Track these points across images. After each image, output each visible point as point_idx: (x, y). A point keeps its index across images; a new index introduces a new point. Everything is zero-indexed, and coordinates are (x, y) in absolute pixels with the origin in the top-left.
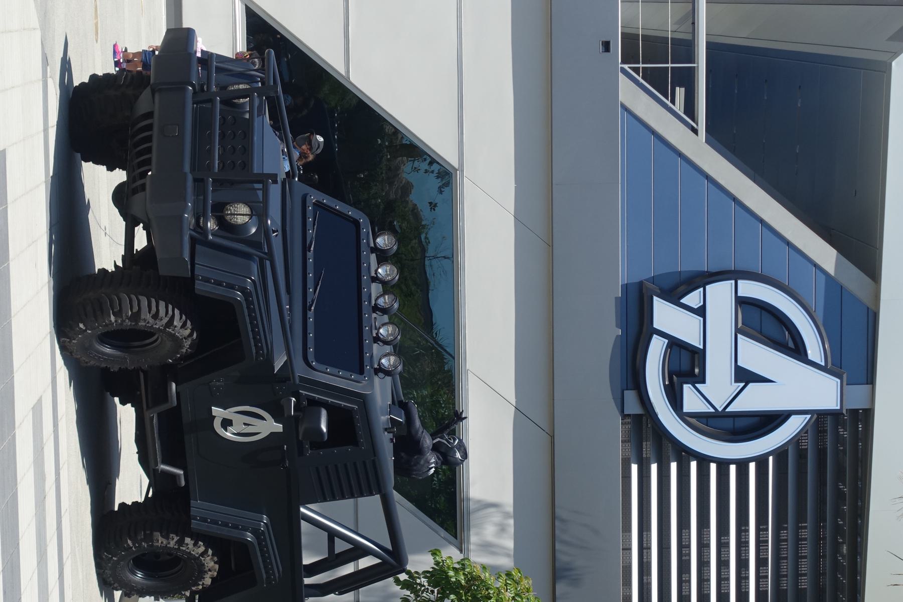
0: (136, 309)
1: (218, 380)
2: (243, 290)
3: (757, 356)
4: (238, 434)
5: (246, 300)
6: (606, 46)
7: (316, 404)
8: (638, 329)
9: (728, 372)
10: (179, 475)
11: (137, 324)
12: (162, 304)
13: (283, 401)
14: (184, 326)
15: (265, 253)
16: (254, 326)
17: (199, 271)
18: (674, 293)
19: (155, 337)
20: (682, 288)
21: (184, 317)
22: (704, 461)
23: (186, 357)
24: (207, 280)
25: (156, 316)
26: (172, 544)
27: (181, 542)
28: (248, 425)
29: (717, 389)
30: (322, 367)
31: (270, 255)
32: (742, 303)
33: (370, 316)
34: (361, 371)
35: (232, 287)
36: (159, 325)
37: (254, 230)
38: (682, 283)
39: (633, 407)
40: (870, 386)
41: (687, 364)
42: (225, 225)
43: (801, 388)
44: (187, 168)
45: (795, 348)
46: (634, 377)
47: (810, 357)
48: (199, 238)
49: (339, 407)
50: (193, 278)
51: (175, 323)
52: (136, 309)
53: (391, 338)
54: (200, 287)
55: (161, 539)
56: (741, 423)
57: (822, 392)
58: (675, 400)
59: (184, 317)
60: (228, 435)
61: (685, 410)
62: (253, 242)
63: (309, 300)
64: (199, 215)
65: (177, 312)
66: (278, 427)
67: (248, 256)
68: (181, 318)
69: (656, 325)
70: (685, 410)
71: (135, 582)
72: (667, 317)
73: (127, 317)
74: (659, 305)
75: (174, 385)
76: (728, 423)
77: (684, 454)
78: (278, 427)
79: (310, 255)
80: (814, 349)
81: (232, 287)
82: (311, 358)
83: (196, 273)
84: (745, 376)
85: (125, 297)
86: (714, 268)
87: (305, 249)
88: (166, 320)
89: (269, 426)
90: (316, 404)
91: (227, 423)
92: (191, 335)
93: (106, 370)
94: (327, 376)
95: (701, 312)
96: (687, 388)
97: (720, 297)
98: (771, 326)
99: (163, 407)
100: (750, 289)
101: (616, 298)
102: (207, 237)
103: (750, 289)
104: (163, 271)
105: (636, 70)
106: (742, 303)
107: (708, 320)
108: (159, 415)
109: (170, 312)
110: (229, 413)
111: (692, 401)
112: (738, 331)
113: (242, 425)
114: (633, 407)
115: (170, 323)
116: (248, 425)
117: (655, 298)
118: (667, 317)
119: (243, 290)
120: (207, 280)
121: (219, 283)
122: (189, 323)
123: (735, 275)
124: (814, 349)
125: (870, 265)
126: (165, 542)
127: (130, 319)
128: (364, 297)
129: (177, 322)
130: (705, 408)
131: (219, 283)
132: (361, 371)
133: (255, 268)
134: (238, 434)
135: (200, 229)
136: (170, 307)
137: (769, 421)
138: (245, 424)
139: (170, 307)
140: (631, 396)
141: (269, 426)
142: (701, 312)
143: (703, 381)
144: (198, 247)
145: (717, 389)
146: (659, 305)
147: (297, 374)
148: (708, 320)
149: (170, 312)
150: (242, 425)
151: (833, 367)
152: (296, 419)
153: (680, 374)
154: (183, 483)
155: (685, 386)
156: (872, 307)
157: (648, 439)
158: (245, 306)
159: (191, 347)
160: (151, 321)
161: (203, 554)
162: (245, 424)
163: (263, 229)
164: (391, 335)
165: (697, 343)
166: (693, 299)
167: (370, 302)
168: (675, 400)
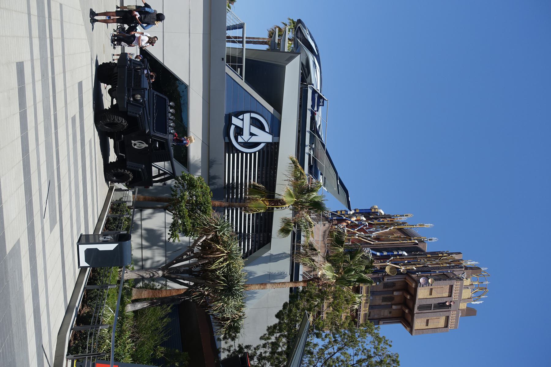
3: (254, 130)
8: (229, 123)
9: (248, 134)
17: (129, 110)
18: (237, 116)
22: (242, 153)
25: (118, 120)
27: (124, 171)
29: (246, 137)
31: (145, 107)
34: (166, 133)
39: (227, 141)
41: (239, 131)
42: (134, 99)
43: (264, 137)
44: (126, 86)
45: (262, 128)
50: (127, 111)
57: (268, 138)
62: (141, 104)
66: (147, 146)
67: (140, 107)
72: (235, 120)
77: (238, 151)
78: (147, 146)
80: (267, 129)
81: (136, 114)
84: (252, 134)
87: (153, 105)
89: (145, 145)
91: (135, 144)
95: (243, 120)
96: (239, 137)
97: (247, 116)
100: (253, 115)
103: (253, 115)
110: (136, 142)
111: (240, 140)
113: (138, 145)
114: (227, 141)
118: (235, 120)
123: (250, 112)
124: (267, 129)
132: (166, 133)
140: (226, 138)
141: (145, 145)
142: (243, 120)
145: (246, 137)
148: (244, 121)
150: (138, 145)
151: (270, 133)
157: (230, 148)
166: (241, 117)
168: (236, 139)
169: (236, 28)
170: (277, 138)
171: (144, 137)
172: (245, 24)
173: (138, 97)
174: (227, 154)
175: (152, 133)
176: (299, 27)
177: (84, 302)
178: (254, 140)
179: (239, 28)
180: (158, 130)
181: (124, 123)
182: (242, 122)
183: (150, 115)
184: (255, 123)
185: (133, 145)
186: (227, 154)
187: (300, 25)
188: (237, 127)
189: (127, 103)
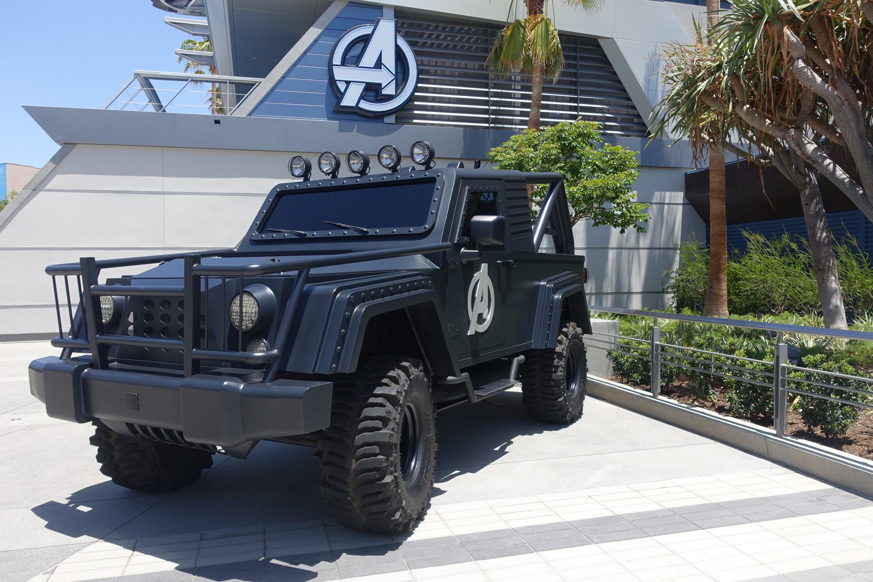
0: (376, 449)
1: (448, 329)
2: (352, 304)
3: (369, 59)
5: (364, 300)
7: (468, 228)
8: (355, 113)
9: (376, 72)
11: (395, 445)
12: (367, 412)
14: (395, 380)
15: (300, 274)
18: (340, 96)
20: (335, 90)
21: (385, 381)
22: (416, 89)
23: (426, 371)
24: (338, 355)
25: (385, 421)
26: (562, 363)
27: (560, 356)
29: (385, 78)
31: (302, 267)
32: (344, 63)
33: (371, 176)
34: (432, 180)
35: (347, 320)
36: (396, 415)
37: (269, 291)
41: (373, 91)
42: (263, 328)
43: (385, 38)
44: (176, 382)
45: (365, 40)
46: (379, 116)
48: (278, 369)
49: (469, 203)
51: (394, 393)
52: (376, 449)
53: (394, 155)
54: (349, 366)
55: (559, 373)
56: (400, 70)
58: (389, 98)
59: (385, 381)
60: (489, 317)
62: (284, 289)
63: (356, 234)
64: (243, 368)
65: (379, 390)
66: (484, 267)
67: (304, 297)
68: (386, 385)
69: (354, 105)
71: (579, 389)
72: (350, 99)
73: (387, 460)
74: (344, 103)
75: (449, 378)
76: (400, 76)
77: (412, 98)
78: (484, 267)
79: (309, 234)
81: (347, 320)
82: (420, 230)
83: (326, 371)
84: (379, 65)
85: (359, 439)
87: (302, 239)
88: (389, 407)
89: (482, 280)
90: (468, 228)
91: (481, 319)
92: (405, 370)
94: (440, 212)
96: (384, 92)
97: (341, 74)
100: (337, 59)
101: (341, 129)
102: (275, 357)
103: (337, 59)
104: (325, 424)
105: (230, 110)
106: (344, 63)
107: (353, 81)
110: (473, 317)
111: (390, 90)
114: (391, 119)
115: (393, 400)
117: (343, 103)
118: (350, 99)
119: (352, 304)
120: (338, 355)
122: (391, 373)
123: (330, 65)
124: (366, 30)
126: (561, 369)
127: (388, 456)
128: (353, 182)
129: (392, 390)
132: (432, 180)
133: (319, 288)
135: (263, 365)
136: (372, 400)
137: (400, 56)
139: (372, 400)
140: (387, 120)
141: (482, 280)
142: (348, 83)
143: (380, 85)
144: (290, 368)
145: (385, 78)
146: (344, 103)
147: (440, 243)
148: (353, 81)
152: (482, 248)
153: (377, 96)
154: (522, 357)
157: (403, 114)
159: (417, 367)
160: (392, 425)
161: (567, 336)
163: (264, 277)
165: (363, 86)
166: (342, 87)
168: (389, 98)
169: (154, 92)
170: (385, 10)
171: (451, 276)
173: (247, 309)
174: (415, 121)
175: (434, 241)
177: (645, 382)
178: (389, 61)
179: (151, 86)
180: (421, 212)
182: (352, 85)
183: (350, 251)
184: (352, 58)
185: (483, 328)
186: (415, 121)
188: (362, 97)
189: (282, 374)
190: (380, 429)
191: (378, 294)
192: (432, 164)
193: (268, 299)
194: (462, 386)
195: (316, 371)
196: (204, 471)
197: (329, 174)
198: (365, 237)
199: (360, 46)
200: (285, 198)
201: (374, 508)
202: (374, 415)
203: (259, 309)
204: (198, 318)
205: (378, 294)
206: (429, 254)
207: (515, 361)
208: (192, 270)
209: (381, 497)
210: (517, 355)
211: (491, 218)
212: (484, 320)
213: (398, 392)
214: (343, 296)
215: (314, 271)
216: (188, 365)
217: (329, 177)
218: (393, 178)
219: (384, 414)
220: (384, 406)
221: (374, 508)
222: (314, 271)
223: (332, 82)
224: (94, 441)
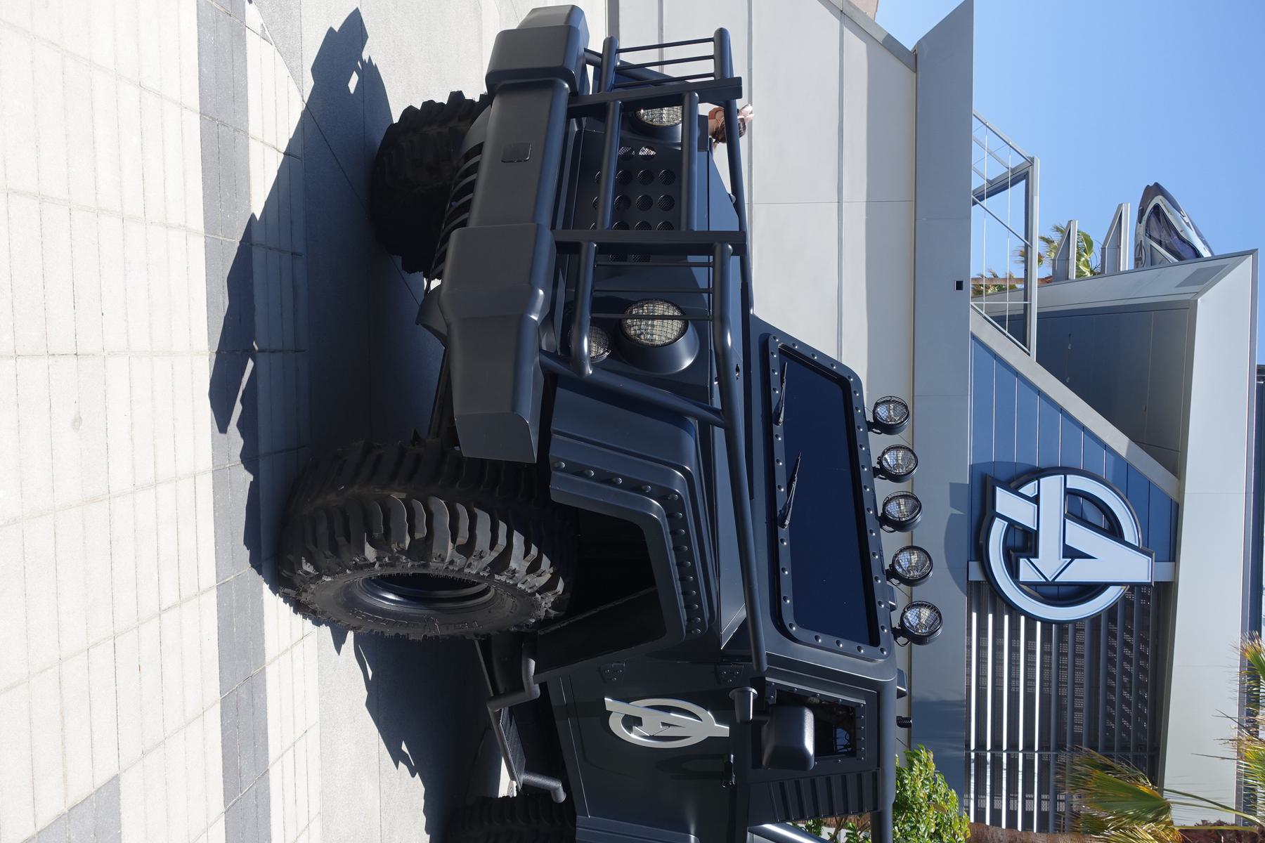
0: (421, 534)
2: (665, 496)
3: (1080, 537)
4: (652, 738)
5: (670, 516)
6: (959, 285)
7: (801, 701)
8: (984, 513)
9: (1057, 550)
10: (556, 789)
11: (426, 566)
12: (484, 519)
13: (734, 694)
14: (534, 568)
15: (715, 411)
16: (683, 557)
17: (560, 453)
18: (1013, 486)
19: (484, 586)
21: (534, 550)
22: (1031, 619)
23: (547, 622)
25: (467, 549)
28: (669, 725)
29: (1047, 563)
30: (808, 635)
31: (726, 412)
32: (1070, 493)
33: (878, 534)
34: (874, 640)
35: (636, 487)
36: (476, 567)
37: (687, 362)
38: (1019, 476)
39: (976, 574)
40: (1171, 564)
41: (1023, 543)
42: (627, 351)
43: (1118, 565)
44: (545, 219)
45: (1113, 531)
46: (980, 553)
47: (1127, 539)
48: (560, 375)
50: (543, 468)
54: (562, 490)
56: (1063, 590)
57: (1134, 567)
58: (1013, 571)
59: (534, 550)
61: (1021, 579)
62: (690, 386)
63: (779, 508)
64: (564, 320)
65: (518, 539)
66: (723, 730)
67: (677, 418)
68: (527, 552)
70: (1021, 579)
72: (1005, 502)
73: (402, 552)
74: (1000, 492)
75: (533, 663)
76: (1054, 590)
77: (1015, 611)
78: (723, 730)
80: (1130, 531)
81: (636, 487)
82: (788, 617)
83: (553, 453)
84: (1071, 554)
86: (1043, 465)
87: (770, 418)
88: (490, 557)
89: (700, 726)
90: (801, 701)
91: (632, 722)
92: (550, 586)
93: (400, 640)
94: (819, 652)
95: (1036, 500)
96: (1023, 561)
97: (1051, 488)
98: (1092, 514)
99: (517, 699)
100: (1075, 482)
102: (581, 369)
103: (1075, 482)
105: (980, 306)
107: (1041, 507)
108: (511, 709)
109: (502, 541)
110: (636, 708)
111: (1027, 572)
112: (1065, 516)
113: (655, 724)
114: (976, 574)
115: (501, 563)
116: (669, 725)
118: (1005, 502)
119: (665, 496)
121: (606, 479)
122: (546, 562)
123: (1065, 471)
124: (1130, 531)
125: (1174, 462)
127: (408, 553)
128: (867, 503)
129: (518, 563)
130: (1036, 578)
131: (606, 479)
132: (874, 640)
133: (691, 444)
134: (652, 738)
135: (567, 352)
136: (503, 528)
137: (1089, 591)
138: (664, 724)
139: (503, 528)
140: (974, 567)
141: (700, 726)
142: (1036, 500)
143: (1036, 556)
144: (561, 393)
145: (1047, 563)
146: (1000, 492)
147: (765, 652)
148: (1041, 507)
149: (502, 541)
150: (655, 724)
151: (1144, 549)
152: (756, 726)
153: (1015, 550)
154: (562, 797)
155: (1022, 561)
156: (1175, 498)
157: (986, 596)
158: (666, 529)
159: (555, 606)
160: (460, 560)
162: (664, 724)
164: (916, 568)
167: (876, 512)
168: (1013, 571)
169: (1004, 188)
171: (706, 670)
172: (1038, 163)
173: (660, 328)
174: (974, 615)
175: (769, 641)
176: (1157, 207)
178: (1078, 572)
180: (819, 617)
181: (528, 576)
184: (1080, 508)
185: (616, 725)
186: (974, 615)
187: (1158, 200)
188: (1012, 524)
189: (552, 381)
190: (454, 541)
191: (680, 541)
192: (902, 640)
193: (675, 360)
194: (517, 684)
195: (555, 436)
196: (399, 260)
197: (880, 463)
198: (774, 521)
199: (1103, 523)
200: (837, 390)
201: (323, 529)
202: (478, 532)
203: (658, 346)
204: (645, 252)
205: (680, 541)
206: (746, 631)
207: (556, 785)
208: (723, 243)
209: (341, 540)
210: (566, 788)
211: (809, 744)
212: (630, 729)
213: (514, 571)
214: (677, 482)
215: (719, 434)
216: (570, 236)
217: (875, 464)
218: (876, 572)
219: (478, 548)
220: (492, 548)
221: (323, 529)
222: (719, 434)
223: (1037, 473)
224: (457, 97)
